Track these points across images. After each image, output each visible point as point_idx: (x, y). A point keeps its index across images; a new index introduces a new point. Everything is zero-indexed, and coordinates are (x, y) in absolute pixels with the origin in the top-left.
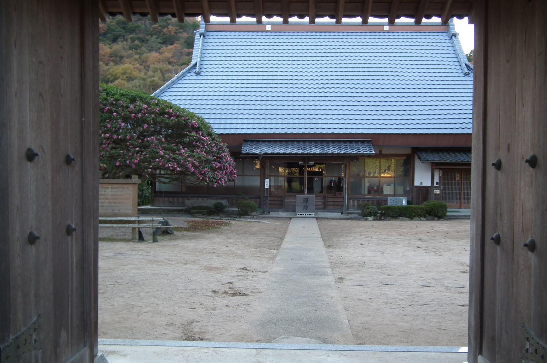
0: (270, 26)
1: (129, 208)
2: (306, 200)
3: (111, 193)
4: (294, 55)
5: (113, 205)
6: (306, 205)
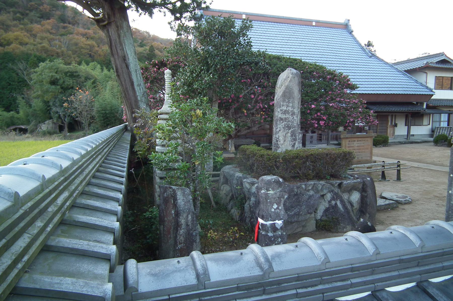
2: (312, 137)
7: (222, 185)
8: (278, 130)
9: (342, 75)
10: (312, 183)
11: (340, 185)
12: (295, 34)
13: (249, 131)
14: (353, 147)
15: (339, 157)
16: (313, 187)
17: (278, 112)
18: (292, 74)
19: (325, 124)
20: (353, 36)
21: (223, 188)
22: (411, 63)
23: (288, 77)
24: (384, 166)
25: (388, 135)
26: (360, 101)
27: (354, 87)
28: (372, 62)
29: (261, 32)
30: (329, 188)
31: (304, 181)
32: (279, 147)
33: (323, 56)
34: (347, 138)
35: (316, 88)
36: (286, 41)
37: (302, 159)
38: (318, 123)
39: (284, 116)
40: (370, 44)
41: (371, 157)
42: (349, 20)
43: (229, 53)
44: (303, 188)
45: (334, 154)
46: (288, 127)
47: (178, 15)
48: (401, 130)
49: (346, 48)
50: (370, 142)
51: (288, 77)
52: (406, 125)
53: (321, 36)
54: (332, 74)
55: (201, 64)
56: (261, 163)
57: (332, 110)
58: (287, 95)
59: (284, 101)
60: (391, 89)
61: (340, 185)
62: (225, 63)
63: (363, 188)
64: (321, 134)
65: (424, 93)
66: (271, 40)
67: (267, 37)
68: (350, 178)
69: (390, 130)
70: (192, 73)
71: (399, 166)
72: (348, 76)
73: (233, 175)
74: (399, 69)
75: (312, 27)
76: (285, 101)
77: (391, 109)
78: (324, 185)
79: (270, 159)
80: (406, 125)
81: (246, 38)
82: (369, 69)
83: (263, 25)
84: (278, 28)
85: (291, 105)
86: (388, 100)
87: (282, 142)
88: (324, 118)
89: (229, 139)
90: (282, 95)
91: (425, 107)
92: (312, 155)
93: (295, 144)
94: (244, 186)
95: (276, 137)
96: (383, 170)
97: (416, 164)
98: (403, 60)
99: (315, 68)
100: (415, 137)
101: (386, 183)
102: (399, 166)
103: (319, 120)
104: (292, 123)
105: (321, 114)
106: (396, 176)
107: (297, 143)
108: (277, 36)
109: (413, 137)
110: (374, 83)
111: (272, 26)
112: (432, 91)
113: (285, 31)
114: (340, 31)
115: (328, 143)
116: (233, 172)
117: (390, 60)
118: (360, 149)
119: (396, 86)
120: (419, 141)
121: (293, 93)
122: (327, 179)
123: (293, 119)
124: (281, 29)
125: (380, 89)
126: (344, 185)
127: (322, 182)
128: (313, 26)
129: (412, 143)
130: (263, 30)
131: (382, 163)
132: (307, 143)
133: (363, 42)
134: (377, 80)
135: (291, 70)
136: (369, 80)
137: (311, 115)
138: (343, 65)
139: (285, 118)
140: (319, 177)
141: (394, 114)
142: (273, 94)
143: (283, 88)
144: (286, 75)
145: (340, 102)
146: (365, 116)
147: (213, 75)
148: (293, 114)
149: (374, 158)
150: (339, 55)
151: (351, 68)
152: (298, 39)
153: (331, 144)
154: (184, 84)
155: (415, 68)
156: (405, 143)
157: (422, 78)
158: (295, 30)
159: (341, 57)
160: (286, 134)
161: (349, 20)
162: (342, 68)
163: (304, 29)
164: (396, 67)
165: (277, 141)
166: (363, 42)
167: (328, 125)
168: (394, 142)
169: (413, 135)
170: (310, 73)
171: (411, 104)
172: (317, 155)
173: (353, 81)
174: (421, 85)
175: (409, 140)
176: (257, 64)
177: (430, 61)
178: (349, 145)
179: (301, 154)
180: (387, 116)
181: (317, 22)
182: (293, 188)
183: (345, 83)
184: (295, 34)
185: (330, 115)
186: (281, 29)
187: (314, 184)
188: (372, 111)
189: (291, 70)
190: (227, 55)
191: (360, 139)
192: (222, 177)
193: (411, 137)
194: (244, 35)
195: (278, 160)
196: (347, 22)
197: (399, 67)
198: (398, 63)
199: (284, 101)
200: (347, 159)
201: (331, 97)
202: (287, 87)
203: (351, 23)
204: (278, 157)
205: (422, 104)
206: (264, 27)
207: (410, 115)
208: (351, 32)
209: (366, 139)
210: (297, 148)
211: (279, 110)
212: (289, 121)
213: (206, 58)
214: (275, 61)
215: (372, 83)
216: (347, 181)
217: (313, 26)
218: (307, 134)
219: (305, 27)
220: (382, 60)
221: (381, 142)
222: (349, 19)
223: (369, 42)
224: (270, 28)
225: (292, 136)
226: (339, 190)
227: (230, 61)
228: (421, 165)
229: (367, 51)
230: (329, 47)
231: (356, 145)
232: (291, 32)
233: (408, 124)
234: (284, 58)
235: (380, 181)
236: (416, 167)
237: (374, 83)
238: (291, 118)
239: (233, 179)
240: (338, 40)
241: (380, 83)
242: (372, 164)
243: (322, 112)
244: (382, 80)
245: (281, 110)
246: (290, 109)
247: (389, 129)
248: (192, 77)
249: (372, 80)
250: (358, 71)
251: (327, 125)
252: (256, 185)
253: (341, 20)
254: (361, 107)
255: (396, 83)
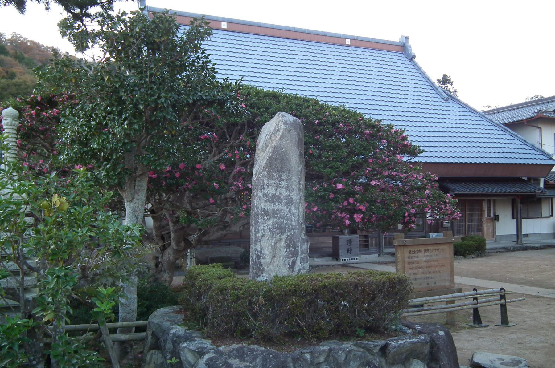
0: (226, 23)
1: (446, 278)
2: (350, 242)
3: (424, 259)
4: (395, 68)
5: (428, 275)
6: (349, 247)
7: (149, 351)
8: (259, 235)
9: (391, 128)
10: (326, 348)
11: (384, 349)
12: (316, 59)
13: (224, 232)
14: (417, 262)
15: (381, 291)
16: (328, 356)
17: (260, 198)
18: (286, 123)
19: (363, 219)
20: (415, 64)
21: (151, 359)
22: (513, 112)
23: (279, 130)
24: (476, 299)
25: (485, 237)
26: (427, 176)
27: (414, 150)
28: (449, 109)
29: (255, 53)
30: (360, 357)
31: (311, 344)
32: (263, 270)
33: (365, 97)
34: (406, 246)
35: (344, 152)
36: (300, 70)
37: (304, 297)
38: (351, 219)
39: (272, 207)
40: (447, 80)
41: (452, 280)
42: (407, 38)
43: (164, 81)
44: (306, 360)
45: (370, 284)
46: (279, 228)
47: (77, 11)
48: (506, 226)
49: (405, 84)
50: (449, 251)
51: (279, 130)
52: (513, 218)
53: (361, 64)
54: (374, 127)
55: (107, 102)
56: (221, 307)
57: (376, 194)
58: (277, 163)
59: (270, 176)
60: (484, 155)
61: (384, 349)
62: (155, 101)
63: (431, 353)
64: (366, 236)
65: (539, 162)
66: (274, 68)
67: (266, 62)
68: (405, 333)
69: (487, 227)
70: (89, 117)
71: (503, 297)
72: (403, 131)
73: (166, 332)
74: (494, 120)
75: (346, 48)
76: (273, 176)
77: (486, 189)
78: (350, 351)
79: (238, 298)
80: (513, 218)
81: (201, 56)
82: (445, 121)
83: (259, 41)
84: (286, 48)
85: (284, 184)
86: (481, 173)
87: (268, 259)
88: (361, 208)
89: (185, 249)
90: (266, 164)
91: (542, 185)
92: (325, 286)
93: (294, 263)
94: (183, 358)
95: (256, 250)
96: (475, 306)
97: (533, 291)
98: (500, 107)
99: (343, 116)
100: (530, 238)
101: (482, 331)
102: (503, 297)
103: (353, 211)
104: (288, 220)
105: (356, 200)
106: (499, 316)
107: (298, 262)
108: (284, 60)
109: (527, 238)
110: (455, 144)
111: (274, 43)
112: (551, 159)
113: (298, 53)
114: (393, 55)
115: (380, 251)
116: (168, 323)
117: (480, 107)
118: (430, 267)
119: (492, 150)
120: (537, 245)
121: (288, 160)
122: (358, 336)
123: (289, 212)
124: (291, 48)
125: (465, 155)
126: (393, 351)
127: (348, 345)
128: (347, 46)
129: (526, 249)
130: (258, 49)
131: (472, 292)
132: (342, 252)
133: (435, 76)
134: (460, 139)
135: (282, 116)
136: (445, 139)
137: (337, 202)
138: (400, 114)
139: (274, 211)
140: (341, 332)
141: (492, 198)
142: (249, 164)
143: (269, 151)
144: (274, 126)
145: (392, 178)
146: (439, 203)
147: (131, 124)
148: (290, 202)
149: (458, 280)
150: (394, 95)
151: (414, 119)
152: (321, 67)
153: (387, 254)
154: (73, 141)
155: (520, 119)
156: (514, 250)
157: (533, 136)
158: (315, 51)
159: (397, 100)
160: (275, 243)
161: (407, 38)
162: (400, 118)
163: (331, 50)
164: (490, 117)
165: (258, 257)
166: (435, 76)
167: (369, 221)
168: (496, 248)
169: (527, 235)
170: (334, 124)
171: (519, 180)
172: (336, 287)
173: (413, 140)
174: (533, 147)
175: (520, 245)
176: (221, 103)
177: (544, 107)
178: (411, 260)
179: (303, 286)
180: (480, 202)
181: (354, 39)
182: (285, 361)
183: (400, 144)
184: (316, 59)
185: (372, 202)
186: (291, 48)
187: (330, 350)
188: (449, 195)
189: (282, 116)
190: (160, 84)
191: (429, 248)
192: (149, 333)
193: (524, 239)
194: (197, 48)
195: (255, 298)
196: (404, 41)
197: (495, 118)
198: (492, 110)
199: (270, 176)
200: (397, 293)
201: (374, 170)
202: (276, 150)
203: (410, 42)
204: (255, 293)
205: (537, 180)
206: (261, 45)
207: (519, 201)
208: (412, 58)
209: (441, 247)
210: (300, 270)
211: (260, 194)
212: (281, 217)
213: (116, 91)
214: (267, 101)
215: (450, 144)
216: (397, 340)
217: (347, 46)
218: (341, 237)
219: (332, 46)
220: (466, 106)
221: (471, 248)
222: (407, 35)
223: (445, 76)
224: (271, 46)
225: (288, 246)
226: (383, 361)
227: (166, 98)
228: (543, 292)
229: (439, 89)
230: (375, 81)
231: (417, 262)
232: (308, 54)
233: (517, 216)
234: (285, 96)
235: (472, 327)
236: (535, 297)
237: (455, 144)
238: (285, 210)
239: (165, 341)
240: (390, 71)
241: (464, 144)
242: (455, 295)
243: (357, 196)
244: (468, 139)
245: (265, 195)
246: (283, 192)
247: (485, 225)
248: (90, 128)
249: (450, 139)
250: (427, 124)
251: (367, 221)
252: (207, 357)
253: (396, 38)
254: (429, 186)
255: (491, 145)
